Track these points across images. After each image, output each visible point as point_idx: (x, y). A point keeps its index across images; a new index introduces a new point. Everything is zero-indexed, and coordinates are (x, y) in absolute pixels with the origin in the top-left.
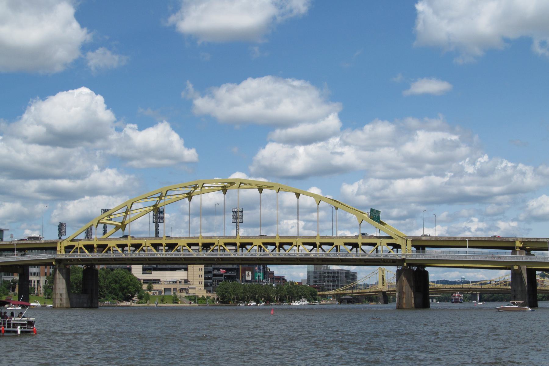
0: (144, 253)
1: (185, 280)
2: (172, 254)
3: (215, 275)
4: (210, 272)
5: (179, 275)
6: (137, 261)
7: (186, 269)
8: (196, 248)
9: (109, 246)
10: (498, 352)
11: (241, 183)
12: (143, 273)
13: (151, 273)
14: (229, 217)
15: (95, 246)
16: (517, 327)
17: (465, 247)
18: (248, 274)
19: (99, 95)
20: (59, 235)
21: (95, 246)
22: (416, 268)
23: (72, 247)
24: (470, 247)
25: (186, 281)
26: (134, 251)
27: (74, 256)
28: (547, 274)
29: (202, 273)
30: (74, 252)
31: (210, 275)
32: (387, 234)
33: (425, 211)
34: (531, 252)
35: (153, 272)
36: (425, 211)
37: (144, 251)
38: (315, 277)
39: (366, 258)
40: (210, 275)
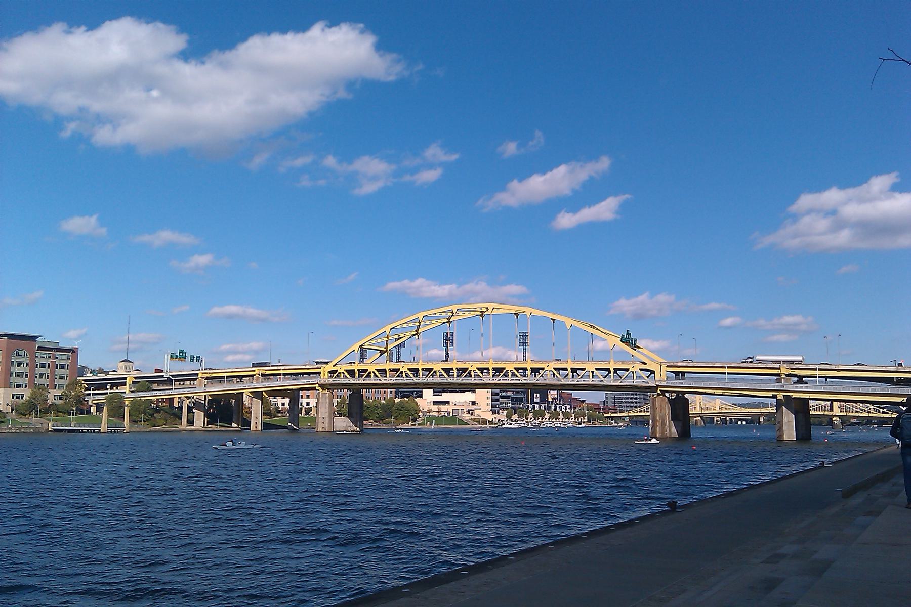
2: (462, 380)
3: (502, 397)
4: (497, 394)
5: (468, 396)
6: (427, 386)
7: (474, 392)
8: (566, 373)
9: (369, 371)
11: (494, 308)
13: (441, 395)
14: (416, 348)
15: (356, 371)
17: (728, 374)
24: (725, 373)
25: (474, 403)
27: (595, 381)
30: (367, 377)
31: (498, 397)
40: (498, 397)
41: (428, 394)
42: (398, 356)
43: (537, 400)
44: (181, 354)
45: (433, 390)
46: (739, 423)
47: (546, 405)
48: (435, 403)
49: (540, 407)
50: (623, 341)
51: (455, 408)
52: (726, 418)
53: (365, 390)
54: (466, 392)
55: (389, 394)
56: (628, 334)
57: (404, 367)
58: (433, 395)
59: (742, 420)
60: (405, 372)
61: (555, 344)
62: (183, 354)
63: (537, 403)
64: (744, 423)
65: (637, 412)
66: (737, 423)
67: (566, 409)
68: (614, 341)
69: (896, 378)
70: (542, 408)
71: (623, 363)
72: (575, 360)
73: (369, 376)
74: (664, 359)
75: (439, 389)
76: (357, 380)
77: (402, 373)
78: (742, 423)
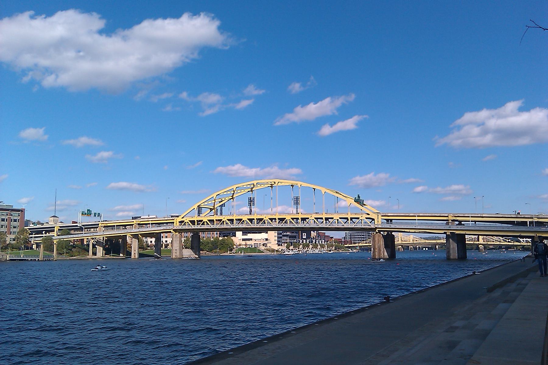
0: (359, 220)
1: (266, 239)
4: (281, 234)
5: (263, 236)
6: (239, 229)
7: (267, 233)
10: (161, 267)
11: (278, 182)
19: (202, 14)
20: (198, 214)
23: (183, 222)
25: (267, 239)
29: (276, 234)
34: (462, 223)
41: (239, 234)
42: (221, 212)
44: (88, 212)
45: (243, 232)
46: (424, 249)
48: (243, 240)
49: (306, 241)
51: (256, 242)
53: (201, 233)
55: (215, 235)
56: (359, 197)
57: (225, 218)
58: (242, 235)
59: (425, 247)
60: (225, 221)
62: (89, 212)
64: (427, 249)
65: (364, 243)
66: (423, 249)
67: (322, 242)
69: (516, 221)
73: (203, 224)
75: (245, 231)
76: (196, 227)
78: (425, 249)
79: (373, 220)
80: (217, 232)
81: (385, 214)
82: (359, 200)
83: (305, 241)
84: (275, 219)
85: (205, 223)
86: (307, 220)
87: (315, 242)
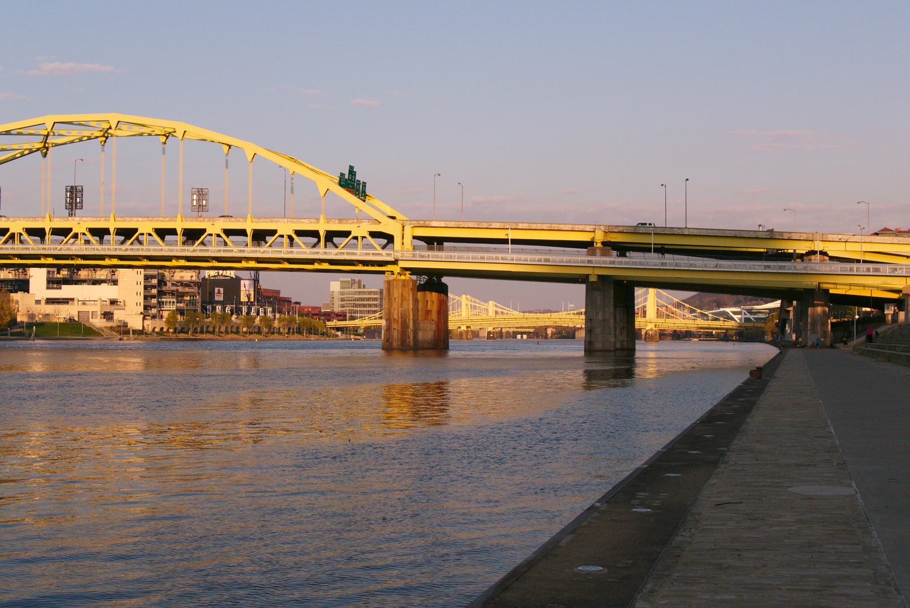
12: (48, 288)
13: (60, 288)
16: (95, 421)
18: (219, 292)
21: (47, 231)
22: (426, 277)
25: (113, 302)
26: (123, 243)
27: (330, 254)
28: (665, 294)
32: (402, 216)
33: (439, 175)
35: (63, 286)
36: (439, 175)
37: (141, 243)
38: (342, 300)
39: (749, 263)
43: (219, 298)
46: (519, 337)
47: (234, 306)
48: (50, 301)
49: (224, 309)
50: (342, 183)
52: (501, 330)
54: (103, 284)
56: (352, 172)
57: (80, 224)
59: (522, 333)
60: (363, 237)
61: (61, 198)
63: (219, 302)
64: (525, 336)
65: (376, 319)
66: (516, 337)
68: (327, 183)
70: (228, 310)
71: (341, 221)
72: (257, 217)
74: (408, 218)
77: (12, 236)
78: (522, 337)
79: (390, 239)
80: (50, 269)
81: (425, 221)
82: (351, 180)
83: (220, 307)
84: (173, 232)
85: (286, 240)
86: (267, 238)
87: (248, 313)
